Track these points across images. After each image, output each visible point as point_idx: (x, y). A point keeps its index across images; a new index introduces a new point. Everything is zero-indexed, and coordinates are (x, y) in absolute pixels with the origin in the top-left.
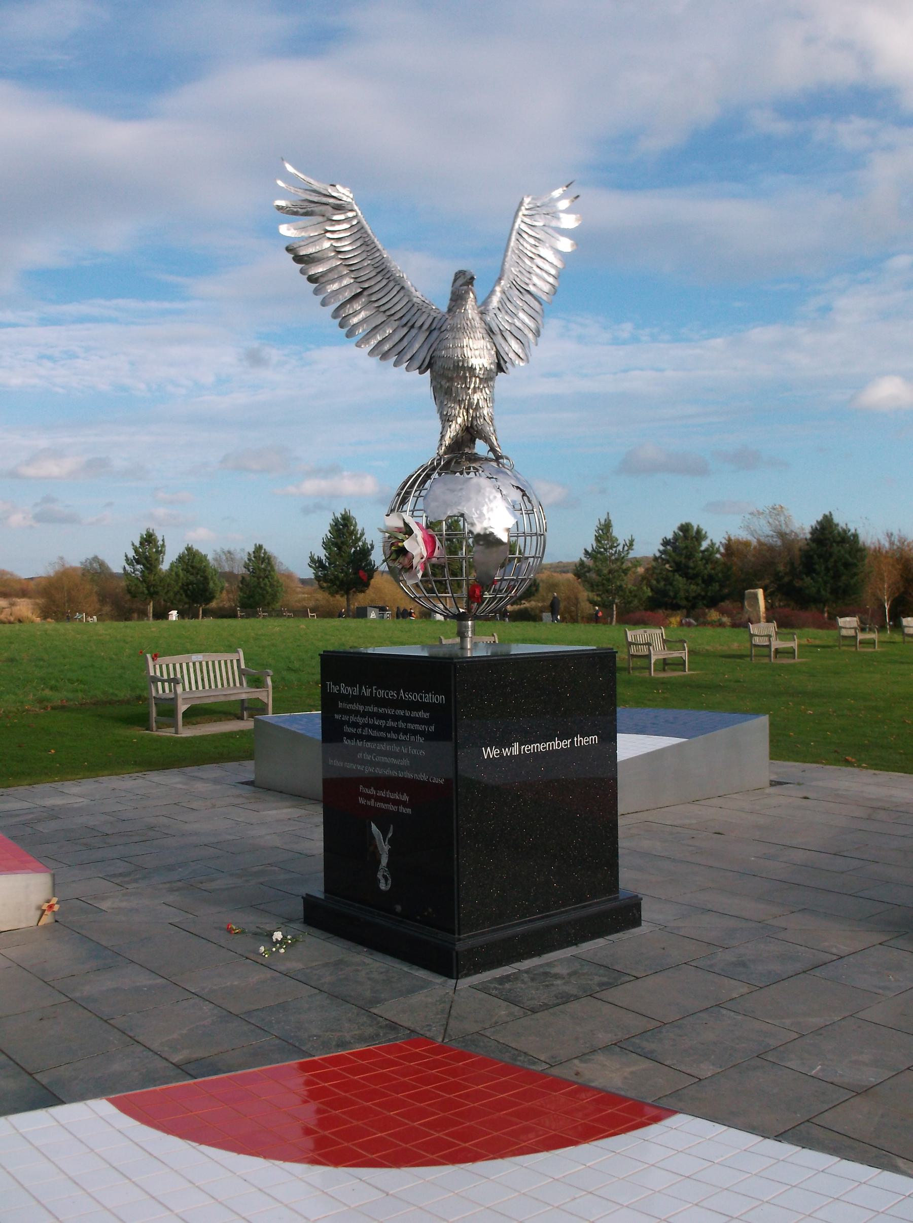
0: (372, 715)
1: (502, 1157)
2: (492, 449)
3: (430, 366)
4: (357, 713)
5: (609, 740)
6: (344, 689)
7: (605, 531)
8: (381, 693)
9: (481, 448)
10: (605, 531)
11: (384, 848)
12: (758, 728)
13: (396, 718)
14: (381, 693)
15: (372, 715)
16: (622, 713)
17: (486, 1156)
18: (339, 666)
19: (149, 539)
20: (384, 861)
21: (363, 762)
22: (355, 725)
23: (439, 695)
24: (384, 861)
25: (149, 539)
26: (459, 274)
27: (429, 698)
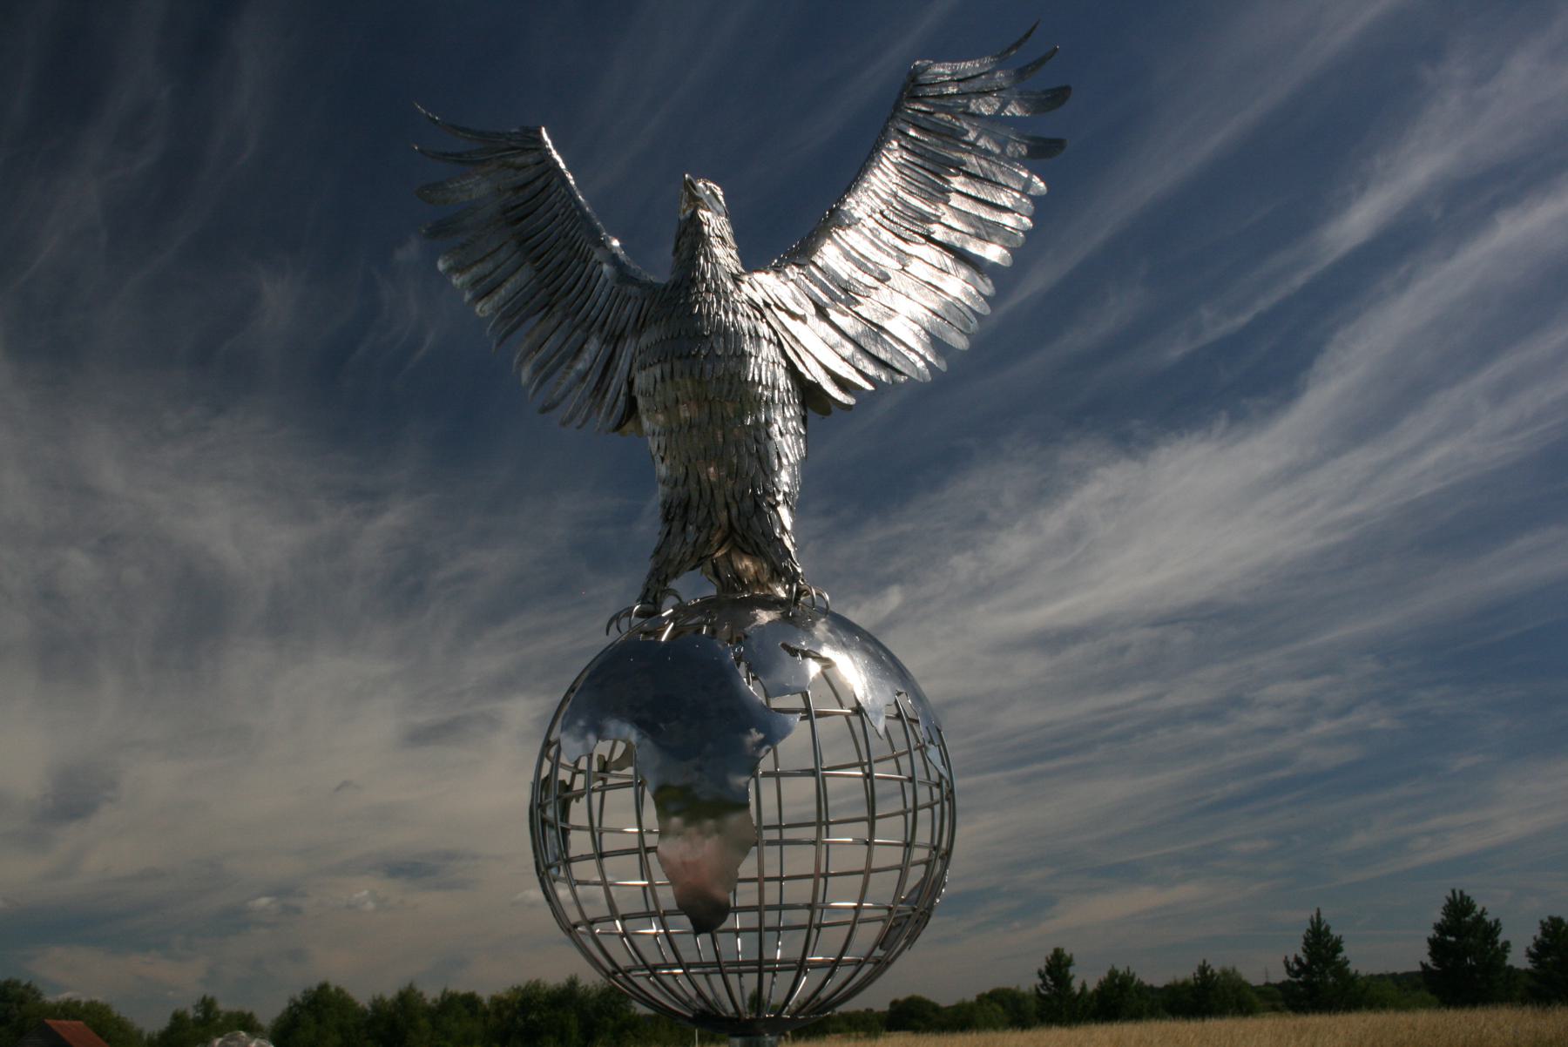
19: (1459, 908)
25: (1459, 908)
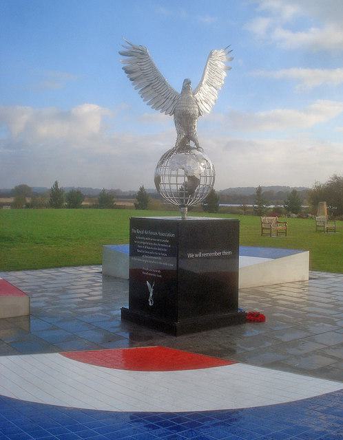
0: (148, 241)
1: (46, 405)
2: (196, 144)
3: (174, 113)
4: (142, 240)
5: (235, 257)
6: (138, 232)
7: (56, 184)
8: (152, 233)
9: (192, 144)
10: (56, 184)
11: (151, 290)
12: (303, 258)
13: (157, 242)
14: (152, 233)
15: (148, 241)
16: (241, 248)
17: (162, 416)
18: (135, 223)
20: (151, 295)
22: (142, 245)
23: (184, 238)
24: (151, 295)
26: (186, 80)
27: (169, 235)
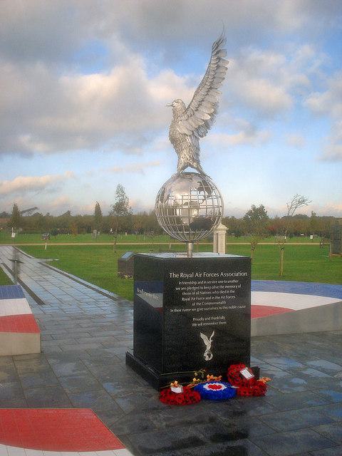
21: (197, 307)
24: (209, 348)
